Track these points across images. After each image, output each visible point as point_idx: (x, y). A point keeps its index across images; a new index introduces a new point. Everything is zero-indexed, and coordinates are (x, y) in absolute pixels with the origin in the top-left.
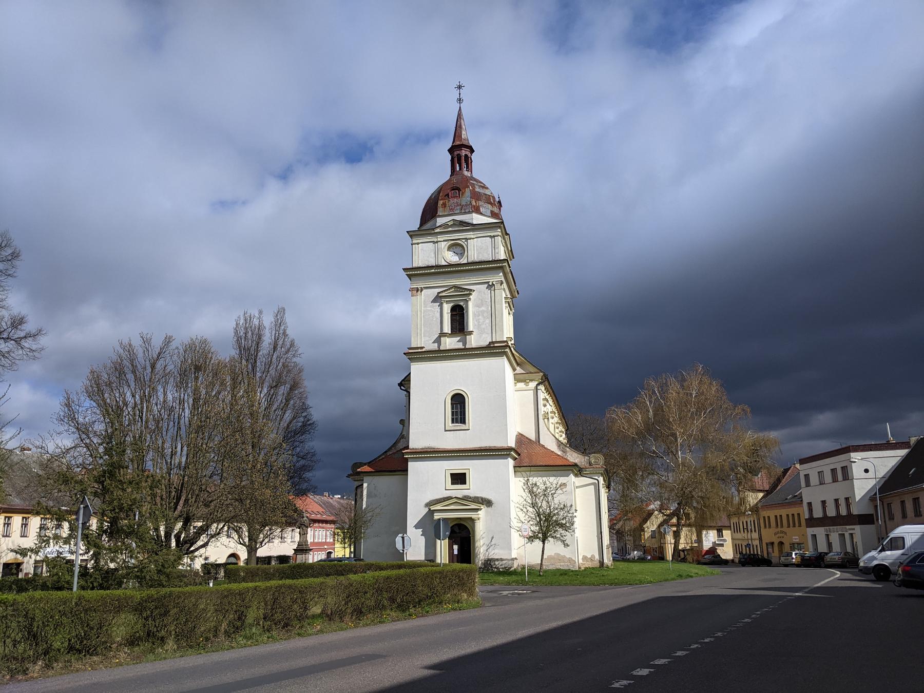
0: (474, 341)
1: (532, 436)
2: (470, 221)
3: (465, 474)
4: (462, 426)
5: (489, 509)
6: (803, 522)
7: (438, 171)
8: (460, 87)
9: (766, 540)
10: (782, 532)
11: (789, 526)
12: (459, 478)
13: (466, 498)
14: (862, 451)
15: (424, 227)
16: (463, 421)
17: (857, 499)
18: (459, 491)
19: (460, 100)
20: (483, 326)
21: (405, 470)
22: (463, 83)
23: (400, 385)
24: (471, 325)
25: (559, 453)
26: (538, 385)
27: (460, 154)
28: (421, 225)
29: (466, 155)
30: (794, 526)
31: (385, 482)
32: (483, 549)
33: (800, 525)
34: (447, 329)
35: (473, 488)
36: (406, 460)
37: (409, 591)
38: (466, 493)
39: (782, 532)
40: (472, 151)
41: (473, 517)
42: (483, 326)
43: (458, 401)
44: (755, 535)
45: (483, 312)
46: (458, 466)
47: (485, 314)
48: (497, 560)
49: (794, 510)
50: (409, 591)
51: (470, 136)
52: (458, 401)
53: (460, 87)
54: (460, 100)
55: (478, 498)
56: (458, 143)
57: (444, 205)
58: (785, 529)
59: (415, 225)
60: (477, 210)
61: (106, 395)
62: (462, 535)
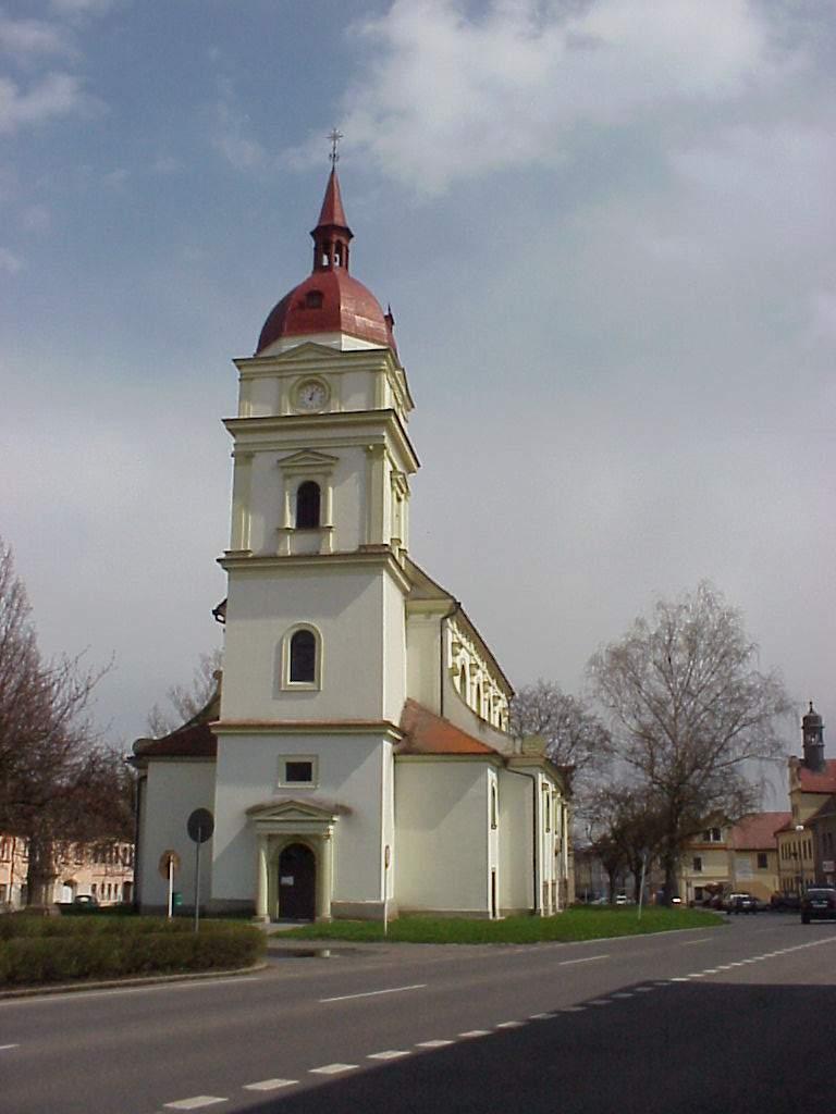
0: (332, 544)
7: (297, 270)
12: (299, 772)
15: (267, 353)
17: (355, 475)
23: (216, 613)
24: (330, 516)
27: (330, 237)
28: (259, 350)
29: (339, 242)
32: (333, 889)
34: (290, 521)
37: (205, 941)
38: (701, 875)
40: (350, 236)
48: (47, 889)
50: (205, 941)
51: (351, 213)
59: (250, 350)
62: (298, 864)
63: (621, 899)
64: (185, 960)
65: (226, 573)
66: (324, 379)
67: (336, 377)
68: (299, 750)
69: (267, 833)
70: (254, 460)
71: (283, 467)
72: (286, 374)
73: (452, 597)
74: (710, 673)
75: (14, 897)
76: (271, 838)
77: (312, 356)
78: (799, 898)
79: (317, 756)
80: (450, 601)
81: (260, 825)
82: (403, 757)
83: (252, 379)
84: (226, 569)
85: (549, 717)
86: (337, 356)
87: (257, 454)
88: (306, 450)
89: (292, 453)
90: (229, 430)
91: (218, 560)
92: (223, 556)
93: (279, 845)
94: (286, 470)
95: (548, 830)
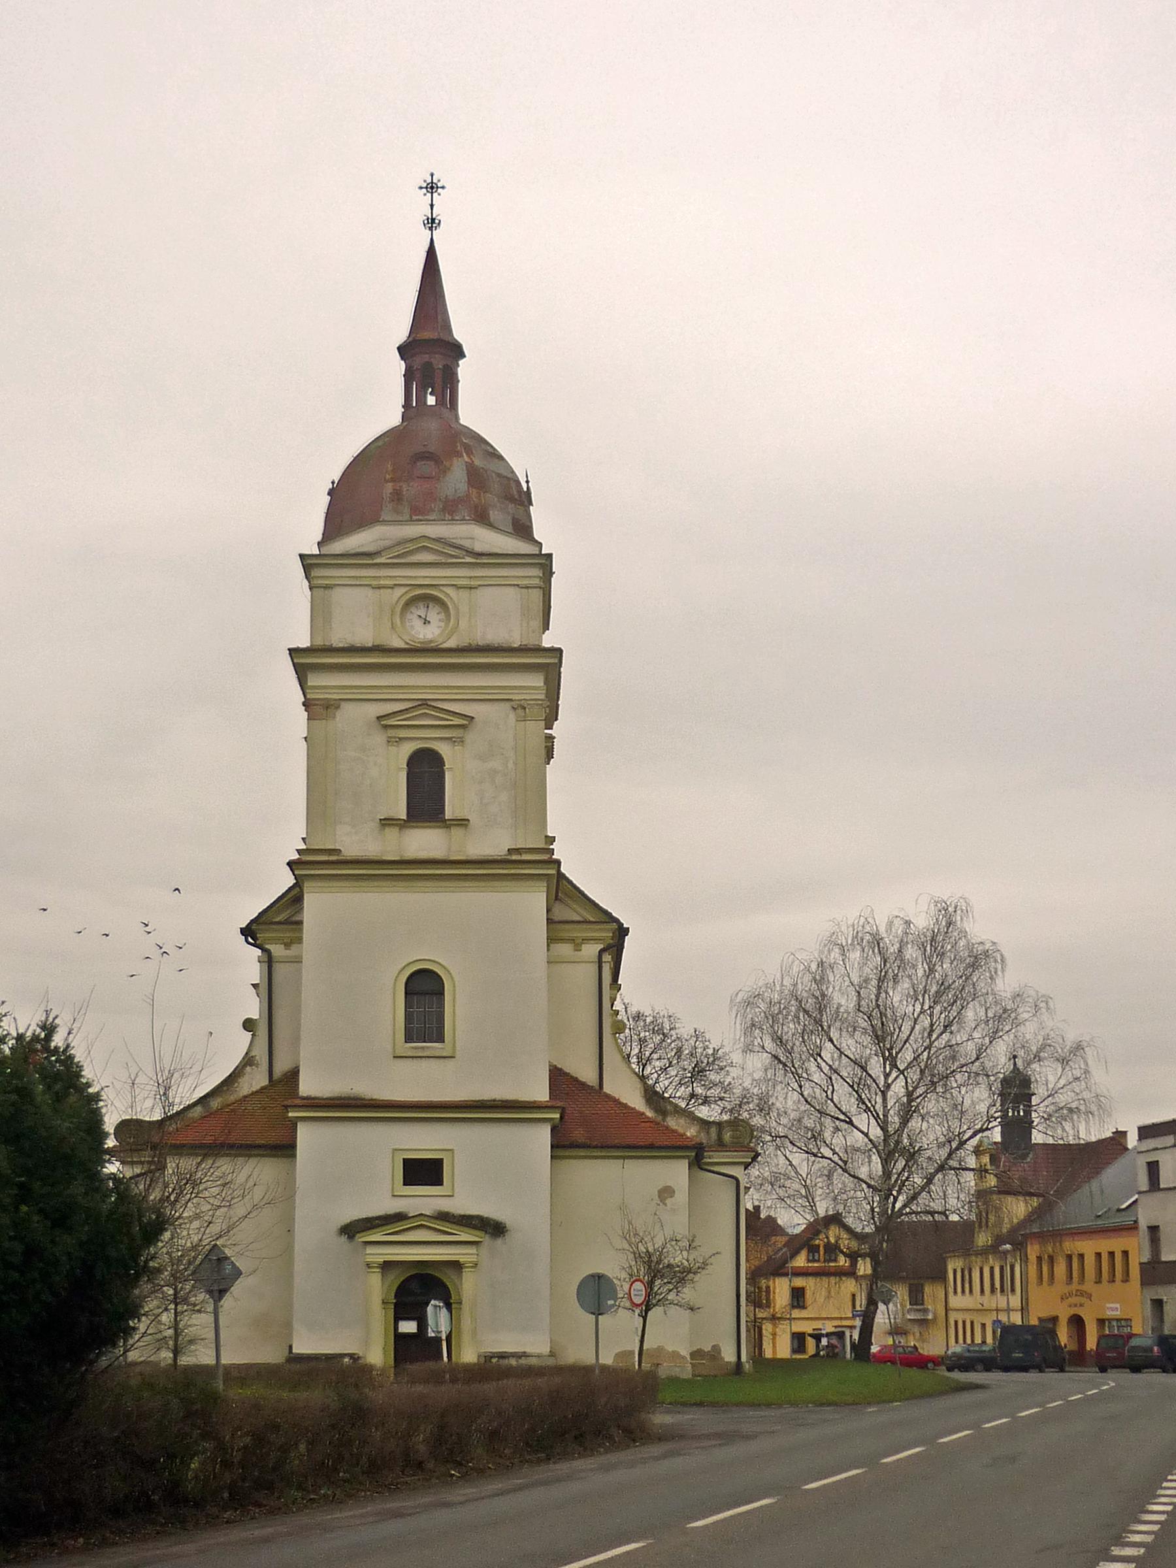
1: (587, 1075)
2: (467, 544)
5: (499, 1241)
6: (1135, 1272)
10: (1081, 1293)
11: (1099, 1281)
12: (423, 1172)
13: (444, 1217)
19: (432, 223)
21: (285, 1149)
22: (441, 177)
25: (650, 1114)
26: (601, 952)
31: (256, 1173)
33: (1126, 1279)
35: (461, 1194)
36: (293, 1125)
39: (1081, 1293)
43: (424, 989)
44: (1015, 1301)
46: (423, 1140)
49: (1116, 1244)
52: (424, 989)
53: (432, 187)
54: (432, 223)
56: (427, 335)
57: (397, 496)
58: (1089, 1286)
60: (482, 517)
61: (938, 1008)
63: (1112, 1309)
66: (447, 595)
67: (464, 594)
68: (423, 1140)
70: (338, 714)
71: (386, 727)
73: (617, 921)
74: (172, 1198)
75: (1134, 1565)
76: (387, 1266)
78: (615, 1299)
80: (615, 926)
81: (370, 1250)
82: (561, 1152)
86: (468, 560)
87: (343, 704)
88: (424, 703)
89: (410, 705)
92: (296, 856)
93: (396, 1278)
94: (391, 733)
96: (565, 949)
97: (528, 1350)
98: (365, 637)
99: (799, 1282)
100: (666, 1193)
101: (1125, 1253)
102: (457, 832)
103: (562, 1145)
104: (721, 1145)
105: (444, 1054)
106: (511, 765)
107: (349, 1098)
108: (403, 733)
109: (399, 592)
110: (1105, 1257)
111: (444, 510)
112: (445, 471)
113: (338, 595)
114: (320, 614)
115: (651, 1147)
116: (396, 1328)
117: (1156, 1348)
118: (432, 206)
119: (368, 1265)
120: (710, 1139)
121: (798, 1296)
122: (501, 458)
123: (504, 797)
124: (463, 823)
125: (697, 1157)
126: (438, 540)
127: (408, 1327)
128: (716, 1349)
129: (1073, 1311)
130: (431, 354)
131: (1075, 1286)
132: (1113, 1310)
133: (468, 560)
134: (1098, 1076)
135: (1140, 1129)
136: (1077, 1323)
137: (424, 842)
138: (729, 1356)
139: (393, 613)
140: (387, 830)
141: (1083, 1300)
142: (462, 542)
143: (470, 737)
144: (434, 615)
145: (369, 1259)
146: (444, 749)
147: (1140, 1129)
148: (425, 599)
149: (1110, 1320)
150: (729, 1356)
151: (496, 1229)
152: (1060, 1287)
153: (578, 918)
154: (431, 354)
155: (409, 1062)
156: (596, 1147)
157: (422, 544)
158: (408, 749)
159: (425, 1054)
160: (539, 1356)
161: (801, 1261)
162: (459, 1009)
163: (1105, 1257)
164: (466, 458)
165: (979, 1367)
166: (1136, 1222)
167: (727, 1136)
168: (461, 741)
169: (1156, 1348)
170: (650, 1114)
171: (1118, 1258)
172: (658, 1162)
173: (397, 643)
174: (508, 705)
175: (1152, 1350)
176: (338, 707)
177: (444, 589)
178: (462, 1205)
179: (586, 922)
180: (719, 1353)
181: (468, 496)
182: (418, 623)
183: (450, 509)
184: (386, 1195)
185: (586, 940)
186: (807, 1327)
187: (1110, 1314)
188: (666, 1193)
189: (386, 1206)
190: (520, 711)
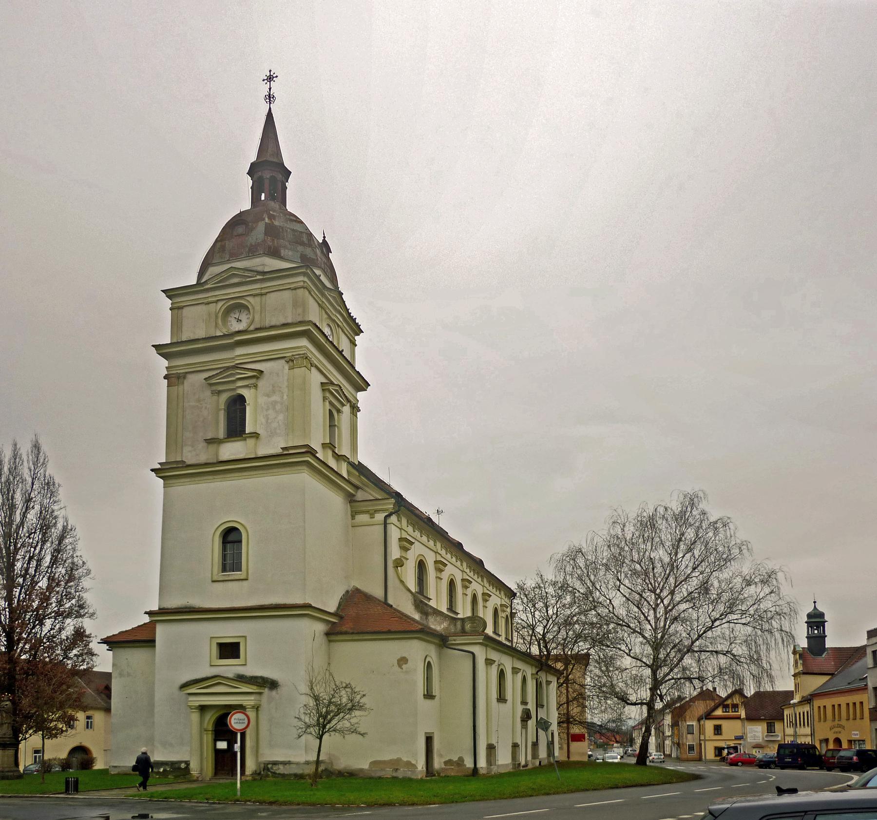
2: (260, 269)
3: (238, 644)
4: (236, 574)
5: (274, 693)
8: (270, 78)
9: (820, 736)
10: (840, 726)
11: (848, 719)
12: (229, 650)
13: (241, 679)
14: (432, 758)
16: (237, 567)
18: (230, 667)
20: (275, 425)
22: (276, 71)
25: (417, 616)
30: (855, 719)
38: (241, 671)
39: (840, 726)
41: (245, 703)
42: (275, 425)
43: (231, 537)
45: (275, 403)
46: (228, 631)
47: (278, 407)
52: (231, 537)
53: (270, 78)
54: (270, 98)
55: (256, 677)
58: (843, 722)
64: (334, 777)
65: (161, 481)
67: (258, 299)
68: (228, 631)
69: (197, 704)
71: (211, 385)
72: (263, 291)
76: (203, 709)
77: (235, 280)
79: (245, 637)
81: (191, 698)
82: (333, 638)
83: (266, 294)
84: (160, 477)
85: (740, 548)
86: (258, 277)
89: (214, 373)
90: (159, 354)
91: (152, 470)
92: (159, 466)
94: (214, 388)
95: (502, 699)
96: (363, 518)
97: (292, 759)
98: (201, 333)
99: (718, 722)
100: (403, 661)
101: (861, 703)
102: (251, 442)
103: (332, 634)
104: (463, 632)
105: (242, 578)
106: (285, 397)
107: (186, 608)
108: (220, 388)
109: (220, 304)
110: (851, 705)
111: (250, 250)
112: (252, 229)
113: (186, 311)
114: (176, 325)
115: (389, 632)
116: (215, 745)
117: (855, 758)
118: (270, 89)
119: (190, 707)
120: (456, 629)
121: (718, 730)
122: (302, 223)
123: (281, 417)
124: (255, 435)
125: (443, 641)
126: (246, 270)
127: (222, 745)
128: (461, 759)
129: (836, 736)
130: (269, 172)
131: (837, 722)
132: (856, 735)
133: (258, 277)
134: (786, 590)
135: (868, 632)
136: (838, 741)
137: (232, 450)
138: (469, 764)
139: (217, 317)
140: (210, 446)
141: (840, 729)
142: (255, 269)
143: (261, 383)
144: (244, 317)
145: (190, 704)
146: (244, 392)
147: (868, 632)
148: (238, 307)
149: (855, 741)
150: (469, 764)
151: (273, 685)
152: (829, 723)
153: (372, 498)
154: (269, 172)
155: (221, 584)
156: (367, 633)
157: (231, 273)
158: (224, 397)
159: (230, 578)
160: (297, 764)
161: (719, 712)
162: (250, 550)
163: (851, 705)
164: (267, 220)
165: (772, 766)
166: (866, 685)
167: (468, 627)
168: (256, 386)
169: (855, 758)
170: (417, 616)
171: (858, 706)
172: (397, 642)
173: (219, 334)
174: (283, 361)
175: (851, 758)
176: (185, 378)
177: (248, 298)
178: (250, 671)
179: (377, 499)
180: (463, 761)
181: (264, 241)
182: (234, 322)
183: (253, 252)
184: (206, 664)
185: (376, 511)
186: (722, 744)
187: (854, 737)
188: (403, 661)
189: (207, 671)
190: (291, 363)
